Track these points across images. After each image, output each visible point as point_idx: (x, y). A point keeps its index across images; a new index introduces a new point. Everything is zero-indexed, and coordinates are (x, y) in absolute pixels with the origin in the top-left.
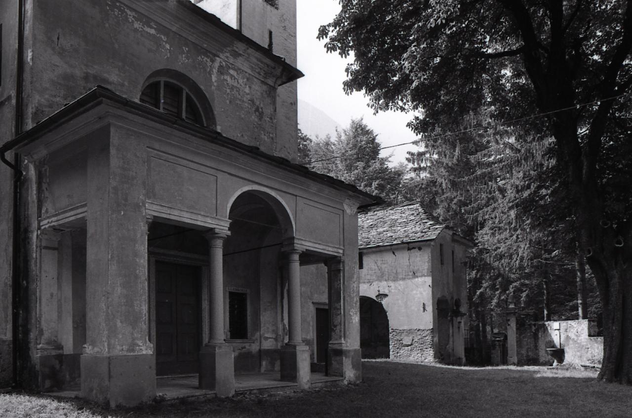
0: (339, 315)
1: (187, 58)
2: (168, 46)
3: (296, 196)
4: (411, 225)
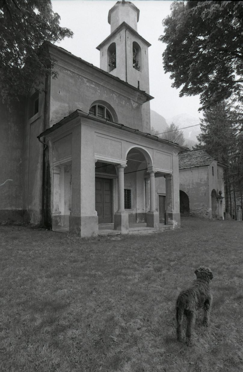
0: (171, 199)
1: (107, 95)
2: (99, 91)
3: (153, 149)
4: (199, 159)
